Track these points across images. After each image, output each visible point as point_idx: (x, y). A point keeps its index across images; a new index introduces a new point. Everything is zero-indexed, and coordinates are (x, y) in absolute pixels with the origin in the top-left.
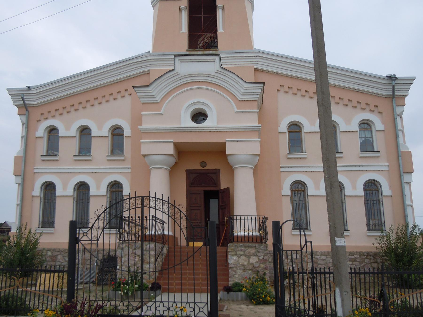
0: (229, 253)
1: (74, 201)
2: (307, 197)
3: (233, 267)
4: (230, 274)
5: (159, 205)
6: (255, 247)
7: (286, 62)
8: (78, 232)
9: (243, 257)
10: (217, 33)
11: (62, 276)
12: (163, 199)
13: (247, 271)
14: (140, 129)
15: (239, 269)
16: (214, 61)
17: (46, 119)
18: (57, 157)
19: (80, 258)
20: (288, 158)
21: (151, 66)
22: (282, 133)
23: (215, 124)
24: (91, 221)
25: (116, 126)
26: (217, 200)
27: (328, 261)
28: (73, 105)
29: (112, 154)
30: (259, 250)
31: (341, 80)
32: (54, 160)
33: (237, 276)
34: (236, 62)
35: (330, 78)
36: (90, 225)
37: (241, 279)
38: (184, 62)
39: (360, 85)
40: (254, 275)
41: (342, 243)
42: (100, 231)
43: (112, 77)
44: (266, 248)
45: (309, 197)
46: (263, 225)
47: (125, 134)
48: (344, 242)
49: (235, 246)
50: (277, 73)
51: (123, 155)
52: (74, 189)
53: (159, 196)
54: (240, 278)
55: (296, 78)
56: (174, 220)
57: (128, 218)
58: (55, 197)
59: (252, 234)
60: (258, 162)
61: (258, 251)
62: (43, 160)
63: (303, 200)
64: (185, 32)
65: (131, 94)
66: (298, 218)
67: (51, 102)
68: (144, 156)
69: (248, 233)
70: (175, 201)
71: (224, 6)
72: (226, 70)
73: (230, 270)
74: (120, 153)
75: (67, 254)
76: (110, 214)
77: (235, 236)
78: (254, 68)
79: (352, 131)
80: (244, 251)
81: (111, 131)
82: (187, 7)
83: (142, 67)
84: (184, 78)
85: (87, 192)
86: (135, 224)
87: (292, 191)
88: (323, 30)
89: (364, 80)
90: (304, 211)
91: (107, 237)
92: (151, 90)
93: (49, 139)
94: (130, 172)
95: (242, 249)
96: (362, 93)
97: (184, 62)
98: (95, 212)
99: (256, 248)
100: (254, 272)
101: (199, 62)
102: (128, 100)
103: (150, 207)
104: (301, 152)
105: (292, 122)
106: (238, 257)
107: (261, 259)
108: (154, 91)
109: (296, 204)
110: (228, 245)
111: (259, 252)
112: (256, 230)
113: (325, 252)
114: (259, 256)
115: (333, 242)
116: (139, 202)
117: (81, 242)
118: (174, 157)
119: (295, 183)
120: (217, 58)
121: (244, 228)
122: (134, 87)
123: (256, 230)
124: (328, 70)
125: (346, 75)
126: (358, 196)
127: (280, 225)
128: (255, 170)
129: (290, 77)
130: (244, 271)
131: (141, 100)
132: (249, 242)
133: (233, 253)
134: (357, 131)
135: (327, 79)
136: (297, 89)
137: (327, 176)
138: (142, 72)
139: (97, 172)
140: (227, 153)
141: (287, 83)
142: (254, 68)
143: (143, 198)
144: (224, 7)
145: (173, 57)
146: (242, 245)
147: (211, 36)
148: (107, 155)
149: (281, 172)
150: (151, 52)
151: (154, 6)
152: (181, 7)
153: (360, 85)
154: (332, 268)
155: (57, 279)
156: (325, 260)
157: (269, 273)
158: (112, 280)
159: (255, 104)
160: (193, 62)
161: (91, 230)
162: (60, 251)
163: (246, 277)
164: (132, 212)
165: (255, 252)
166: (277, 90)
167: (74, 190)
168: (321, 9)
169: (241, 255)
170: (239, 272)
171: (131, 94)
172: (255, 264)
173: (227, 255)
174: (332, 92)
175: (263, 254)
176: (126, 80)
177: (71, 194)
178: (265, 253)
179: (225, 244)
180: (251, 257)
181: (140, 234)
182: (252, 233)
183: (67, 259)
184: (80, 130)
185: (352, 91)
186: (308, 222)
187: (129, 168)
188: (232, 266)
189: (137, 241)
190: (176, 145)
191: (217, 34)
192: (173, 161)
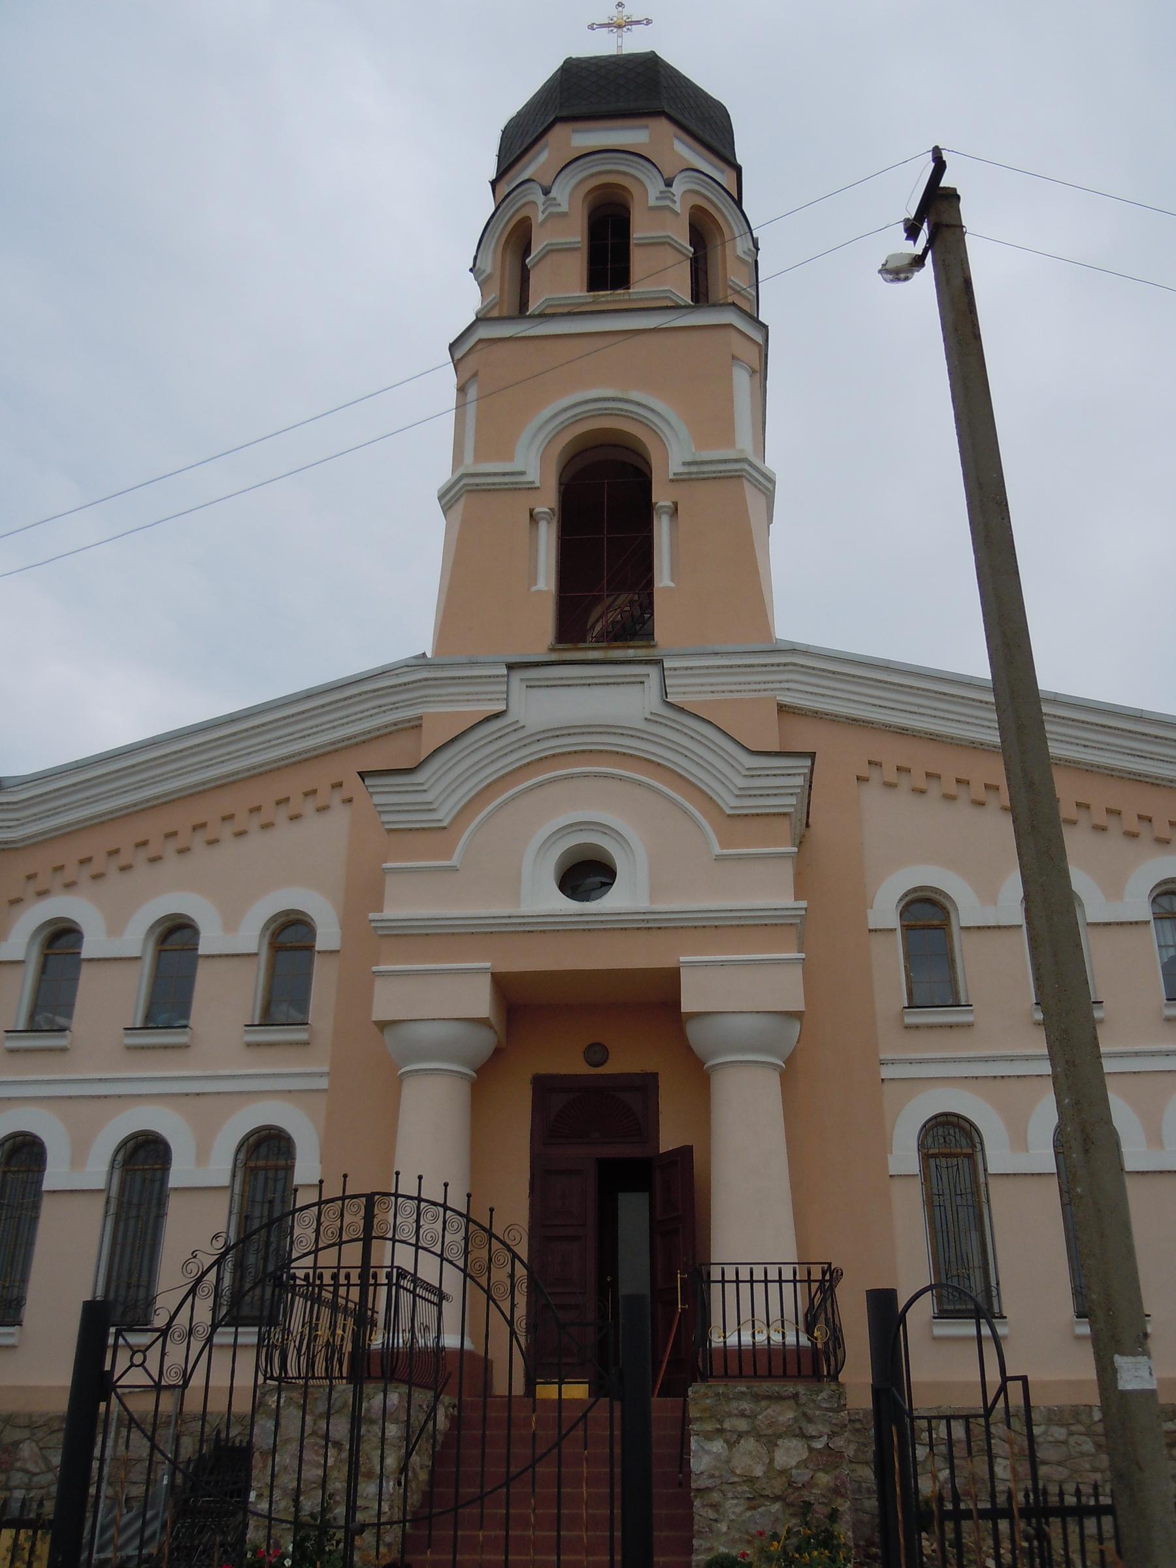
0: (694, 1427)
1: (106, 1212)
2: (982, 1179)
3: (708, 1490)
4: (697, 1518)
5: (431, 1226)
6: (796, 1396)
7: (886, 682)
8: (111, 1341)
9: (749, 1444)
10: (653, 590)
11: (27, 1545)
12: (449, 1204)
13: (764, 1505)
14: (373, 924)
15: (732, 1498)
16: (642, 683)
17: (42, 894)
18: (65, 1037)
19: (108, 1453)
20: (908, 1027)
21: (428, 702)
22: (880, 930)
23: (643, 904)
24: (166, 1300)
25: (288, 915)
26: (646, 1195)
27: (1078, 1449)
28: (145, 843)
29: (267, 1019)
30: (809, 1412)
31: (1077, 741)
32: (50, 1050)
33: (724, 1529)
34: (717, 684)
35: (1052, 739)
36: (160, 1321)
37: (741, 1540)
38: (539, 686)
39: (1145, 758)
40: (794, 1521)
41: (1141, 1377)
42: (196, 1345)
43: (291, 741)
44: (839, 1402)
45: (990, 1181)
46: (824, 1300)
47: (319, 945)
48: (1151, 1374)
49: (718, 1394)
50: (854, 722)
51: (307, 1024)
52: (114, 1160)
53: (433, 1192)
54: (737, 1536)
55: (923, 735)
56: (488, 1292)
57: (304, 1280)
58: (38, 1194)
59: (784, 1343)
60: (798, 1042)
61: (804, 1414)
62: (12, 1051)
63: (969, 1190)
64: (546, 589)
65: (350, 800)
66: (954, 1266)
67: (69, 833)
68: (383, 1025)
69: (769, 1338)
70: (492, 1210)
71: (676, 504)
72: (681, 710)
73: (697, 1503)
74: (295, 1015)
75: (61, 1435)
76: (240, 1267)
77: (717, 1349)
78: (778, 704)
79: (1131, 923)
80: (752, 1417)
81: (268, 933)
82: (556, 510)
83: (396, 705)
84: (538, 741)
85: (158, 1174)
86: (334, 1306)
87: (926, 1157)
88: (1018, 574)
89: (1154, 740)
90: (974, 1235)
91: (221, 1361)
92: (422, 784)
93: (43, 969)
94: (326, 1090)
95: (745, 1406)
96: (1153, 784)
97: (539, 686)
98: (186, 1263)
99: (797, 1403)
100: (791, 1510)
101: (589, 685)
102: (339, 819)
103: (397, 1238)
104: (949, 1003)
105: (915, 890)
106: (726, 1441)
107: (819, 1451)
108: (430, 787)
109: (942, 1208)
110: (690, 1394)
111: (810, 1420)
112: (797, 1323)
113: (1061, 1409)
114: (813, 1437)
115: (1106, 1373)
116: (354, 1219)
117: (116, 1394)
118: (491, 1027)
119: (937, 1125)
120: (653, 672)
121: (753, 1316)
122: (362, 775)
123: (797, 1323)
124: (1043, 711)
125: (1119, 729)
126: (1169, 1172)
127: (900, 1308)
128: (788, 1075)
129: (903, 732)
130: (753, 1502)
131: (385, 818)
132: (770, 1376)
133: (709, 1427)
134: (1147, 923)
135: (1044, 740)
136: (928, 775)
137: (1067, 1101)
138: (395, 724)
139: (203, 1094)
140: (682, 1011)
141: (893, 753)
142: (778, 704)
143: (370, 1199)
144: (677, 509)
145: (504, 671)
146: (744, 1389)
147: (631, 603)
148: (246, 1026)
149: (883, 1080)
150: (429, 655)
151: (446, 509)
152: (537, 510)
153: (1145, 758)
154: (1108, 1488)
155: (5, 1559)
156: (1065, 1442)
157: (855, 1510)
158: (225, 1552)
159: (784, 826)
160: (569, 685)
161: (161, 1339)
162: (33, 1425)
163: (761, 1534)
164: (328, 1258)
165: (795, 1419)
166: (858, 778)
167: (113, 1167)
168: (1007, 505)
169: (740, 1435)
170: (734, 1508)
171: (350, 800)
172: (794, 1471)
173: (683, 1434)
174: (1066, 789)
175: (827, 1430)
176: (337, 751)
177: (101, 1184)
178: (834, 1421)
179: (676, 1388)
180: (780, 1442)
181: (348, 1347)
182: (784, 1338)
183: (56, 1460)
184: (158, 931)
185: (1119, 777)
186: (993, 1283)
187: (321, 1075)
188: (703, 1483)
189: (338, 1378)
190: (502, 984)
191: (651, 595)
192: (485, 1041)
